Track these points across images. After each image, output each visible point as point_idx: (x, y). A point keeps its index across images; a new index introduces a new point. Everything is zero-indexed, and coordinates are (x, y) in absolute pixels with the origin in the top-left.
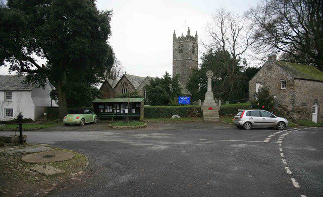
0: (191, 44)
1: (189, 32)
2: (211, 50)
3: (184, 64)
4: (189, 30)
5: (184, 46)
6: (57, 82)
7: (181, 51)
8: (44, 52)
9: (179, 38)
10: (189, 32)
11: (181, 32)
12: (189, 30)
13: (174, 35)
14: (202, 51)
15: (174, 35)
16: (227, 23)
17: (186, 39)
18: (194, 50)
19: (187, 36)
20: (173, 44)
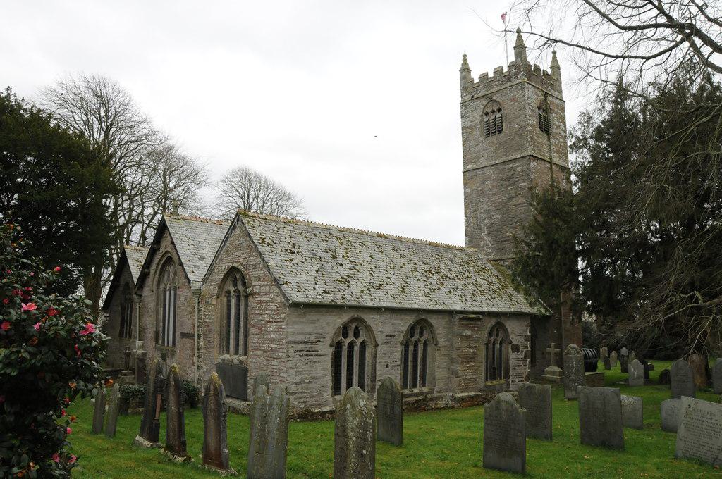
0: (532, 96)
1: (520, 48)
2: (622, 92)
3: (508, 180)
4: (465, 61)
5: (505, 107)
6: (78, 373)
7: (493, 129)
8: (71, 139)
9: (484, 77)
10: (520, 48)
11: (492, 58)
12: (465, 61)
13: (465, 70)
14: (581, 103)
15: (465, 70)
16: (235, 186)
17: (508, 77)
18: (548, 117)
19: (511, 66)
20: (463, 104)
